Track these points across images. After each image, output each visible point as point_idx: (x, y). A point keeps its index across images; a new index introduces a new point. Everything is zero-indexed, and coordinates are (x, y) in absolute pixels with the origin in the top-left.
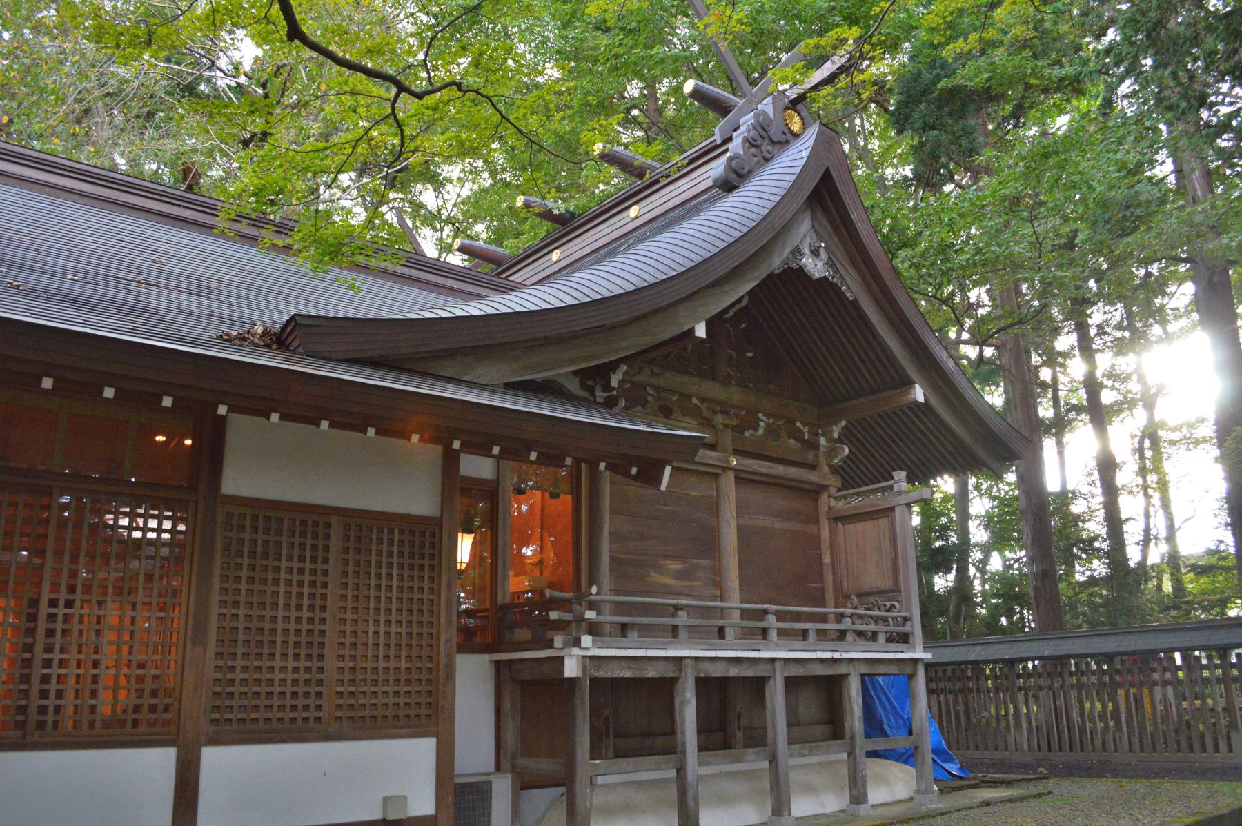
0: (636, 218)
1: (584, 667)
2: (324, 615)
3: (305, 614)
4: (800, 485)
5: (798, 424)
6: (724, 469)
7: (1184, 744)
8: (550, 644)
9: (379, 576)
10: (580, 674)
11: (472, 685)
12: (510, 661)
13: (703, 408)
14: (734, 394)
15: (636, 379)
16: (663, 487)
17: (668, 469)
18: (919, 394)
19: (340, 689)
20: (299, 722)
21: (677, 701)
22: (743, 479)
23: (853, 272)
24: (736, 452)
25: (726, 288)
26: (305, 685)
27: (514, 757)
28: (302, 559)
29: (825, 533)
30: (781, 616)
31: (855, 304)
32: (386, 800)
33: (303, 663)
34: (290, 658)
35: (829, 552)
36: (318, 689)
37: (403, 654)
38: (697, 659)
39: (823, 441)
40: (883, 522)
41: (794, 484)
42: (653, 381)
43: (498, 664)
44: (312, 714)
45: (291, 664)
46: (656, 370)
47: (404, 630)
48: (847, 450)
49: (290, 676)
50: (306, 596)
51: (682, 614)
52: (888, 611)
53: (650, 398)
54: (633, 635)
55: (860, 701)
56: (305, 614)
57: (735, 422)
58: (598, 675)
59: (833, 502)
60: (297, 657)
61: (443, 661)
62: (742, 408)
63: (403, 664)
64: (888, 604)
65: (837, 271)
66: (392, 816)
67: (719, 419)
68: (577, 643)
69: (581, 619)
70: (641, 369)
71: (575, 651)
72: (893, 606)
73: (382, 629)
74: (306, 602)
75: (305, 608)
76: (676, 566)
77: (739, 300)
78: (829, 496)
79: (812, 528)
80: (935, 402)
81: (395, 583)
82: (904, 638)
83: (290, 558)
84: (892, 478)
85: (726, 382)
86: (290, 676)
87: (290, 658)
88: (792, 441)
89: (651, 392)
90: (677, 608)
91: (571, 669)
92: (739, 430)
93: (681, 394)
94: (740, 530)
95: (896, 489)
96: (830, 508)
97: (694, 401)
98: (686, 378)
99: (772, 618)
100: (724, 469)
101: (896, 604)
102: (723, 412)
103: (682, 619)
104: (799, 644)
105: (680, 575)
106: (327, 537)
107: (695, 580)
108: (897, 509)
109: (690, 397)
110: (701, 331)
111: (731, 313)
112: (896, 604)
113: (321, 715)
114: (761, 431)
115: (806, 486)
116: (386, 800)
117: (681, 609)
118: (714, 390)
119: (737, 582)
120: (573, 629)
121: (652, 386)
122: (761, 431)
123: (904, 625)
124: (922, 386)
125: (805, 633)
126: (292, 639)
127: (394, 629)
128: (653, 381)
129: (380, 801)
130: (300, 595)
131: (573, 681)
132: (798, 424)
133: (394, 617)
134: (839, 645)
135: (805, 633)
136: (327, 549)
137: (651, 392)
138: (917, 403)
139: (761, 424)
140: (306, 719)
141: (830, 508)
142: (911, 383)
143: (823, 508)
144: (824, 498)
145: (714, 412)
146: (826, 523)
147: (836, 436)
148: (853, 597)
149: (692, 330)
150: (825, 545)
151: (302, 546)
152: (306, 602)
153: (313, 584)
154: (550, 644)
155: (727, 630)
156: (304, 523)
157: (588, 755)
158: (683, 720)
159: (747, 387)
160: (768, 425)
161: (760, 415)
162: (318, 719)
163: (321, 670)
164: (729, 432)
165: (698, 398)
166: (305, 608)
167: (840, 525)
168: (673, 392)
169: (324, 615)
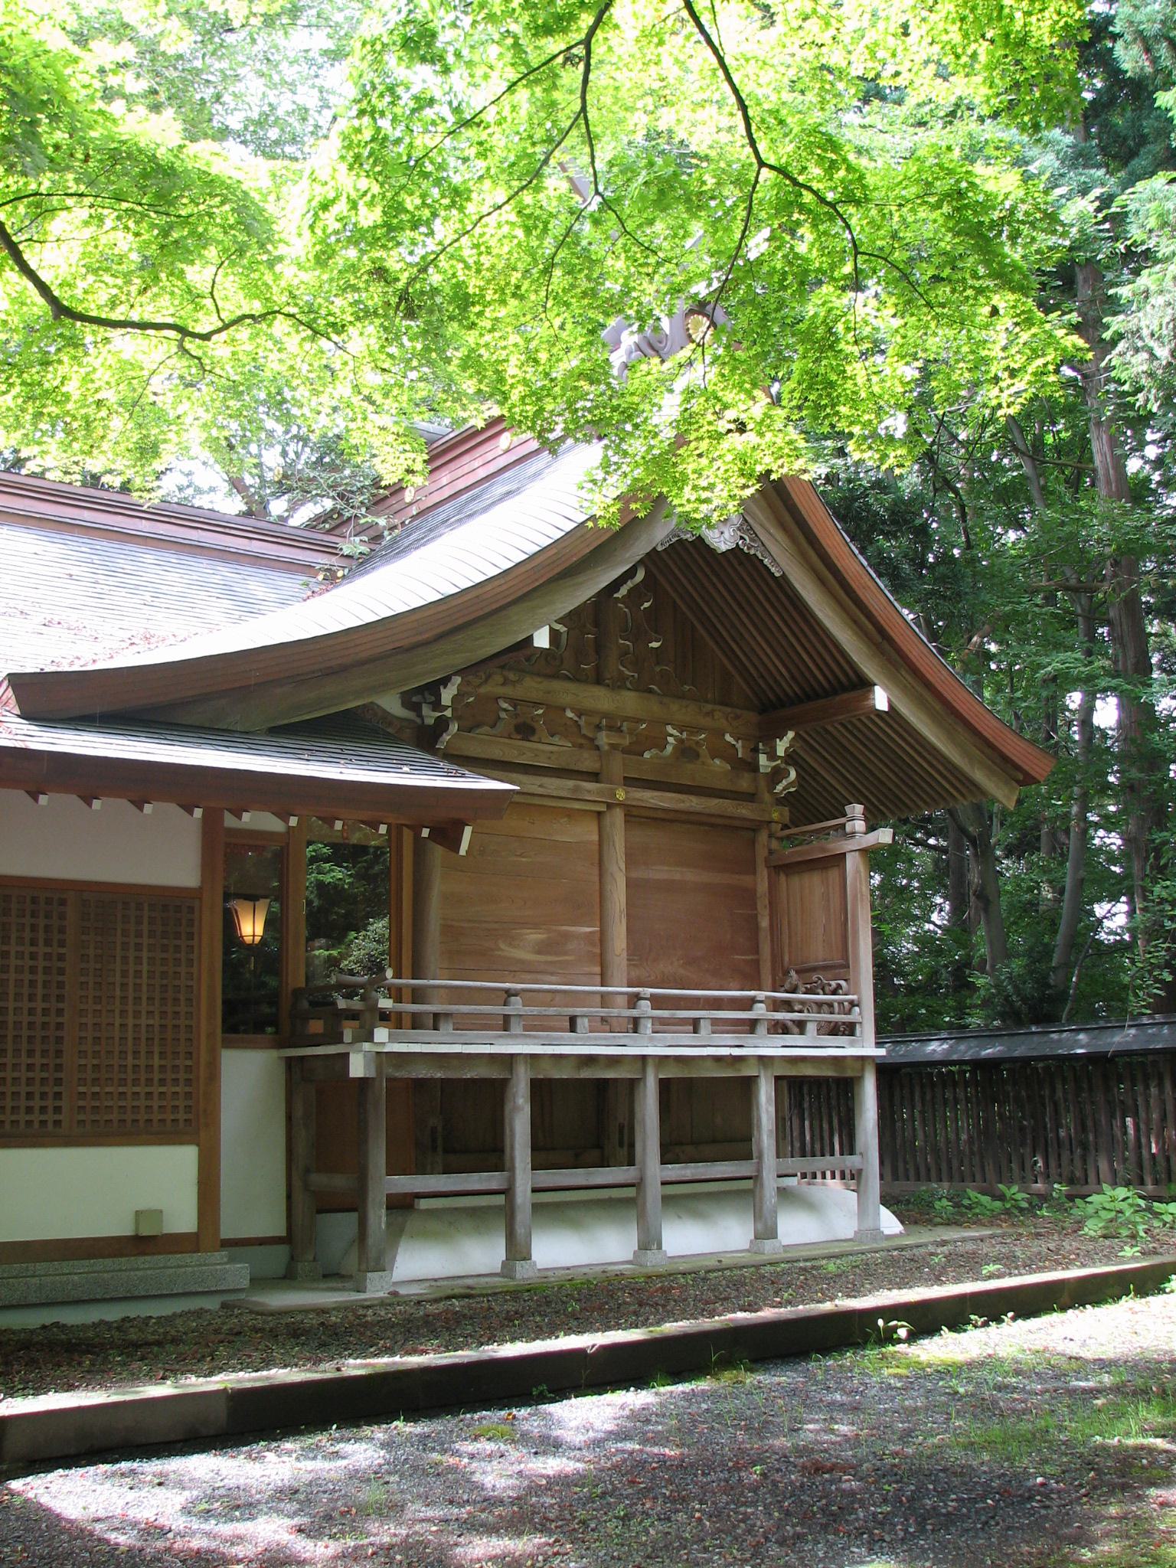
0: (508, 451)
1: (379, 1069)
2: (61, 1005)
3: (40, 1005)
4: (727, 822)
5: (728, 738)
6: (609, 806)
7: (912, 1173)
8: (338, 1039)
9: (125, 959)
10: (372, 1074)
11: (247, 1081)
12: (303, 1058)
13: (582, 722)
14: (628, 702)
15: (482, 690)
16: (463, 851)
17: (468, 831)
18: (881, 699)
19: (82, 1089)
20: (50, 1125)
21: (508, 1107)
22: (635, 816)
23: (779, 535)
24: (629, 782)
25: (581, 579)
26: (42, 1084)
27: (308, 1171)
28: (33, 942)
29: (763, 887)
30: (657, 1002)
31: (783, 582)
32: (138, 1213)
33: (38, 1060)
34: (24, 1053)
35: (767, 912)
36: (57, 1089)
37: (156, 1049)
38: (534, 1057)
39: (763, 759)
40: (833, 874)
41: (713, 820)
42: (508, 691)
43: (290, 1062)
44: (50, 1117)
45: (25, 1060)
46: (512, 676)
47: (156, 1021)
48: (793, 774)
49: (24, 1074)
50: (40, 985)
51: (516, 1000)
52: (834, 993)
53: (503, 715)
54: (447, 1028)
55: (772, 1109)
56: (40, 1005)
57: (626, 741)
58: (398, 1074)
59: (775, 844)
60: (31, 1053)
61: (204, 1057)
62: (640, 721)
63: (156, 1062)
64: (833, 983)
65: (756, 537)
66: (145, 1232)
67: (604, 739)
68: (369, 1038)
69: (374, 1008)
70: (489, 677)
71: (366, 1046)
72: (839, 986)
73: (130, 1021)
74: (40, 991)
75: (39, 997)
76: (534, 936)
77: (630, 573)
78: (770, 836)
79: (746, 880)
80: (907, 710)
81: (145, 968)
82: (850, 1029)
83: (20, 940)
84: (844, 815)
85: (619, 684)
86: (24, 1074)
87: (24, 1053)
88: (717, 761)
89: (505, 705)
90: (509, 993)
91: (358, 1067)
92: (635, 750)
93: (548, 707)
94: (630, 884)
95: (848, 829)
96: (771, 852)
97: (570, 714)
98: (557, 685)
99: (645, 1006)
100: (609, 806)
101: (843, 983)
102: (610, 728)
103: (516, 1006)
104: (688, 1038)
105: (542, 948)
106: (62, 916)
107: (566, 953)
108: (848, 856)
109: (564, 710)
110: (542, 639)
111: (623, 591)
112: (843, 983)
113: (61, 1117)
114: (669, 749)
115: (737, 823)
116: (138, 1213)
117: (516, 995)
118: (601, 699)
119: (624, 954)
120: (367, 1020)
121: (506, 699)
122: (669, 749)
123: (849, 1012)
124: (886, 688)
125: (695, 1024)
126: (25, 1033)
127: (144, 1021)
128: (508, 691)
129: (132, 1216)
130: (33, 984)
131: (363, 1082)
132: (728, 738)
133: (144, 1006)
134: (748, 1039)
135: (695, 1024)
136: (62, 930)
137: (505, 705)
138: (879, 714)
139: (670, 739)
140: (43, 1123)
141: (771, 852)
142: (867, 685)
143: (761, 853)
144: (763, 837)
145: (598, 728)
146: (765, 873)
147: (781, 752)
148: (793, 973)
149: (530, 639)
150: (762, 904)
151: (34, 928)
152: (40, 991)
153: (47, 970)
154: (338, 1039)
155: (579, 1021)
156: (34, 900)
157: (384, 1172)
158: (512, 1130)
159: (650, 691)
160: (680, 741)
161: (670, 729)
162: (57, 1123)
163: (59, 1068)
164: (619, 756)
165: (573, 710)
166: (39, 997)
167: (783, 878)
168: (537, 704)
169: (61, 1005)
